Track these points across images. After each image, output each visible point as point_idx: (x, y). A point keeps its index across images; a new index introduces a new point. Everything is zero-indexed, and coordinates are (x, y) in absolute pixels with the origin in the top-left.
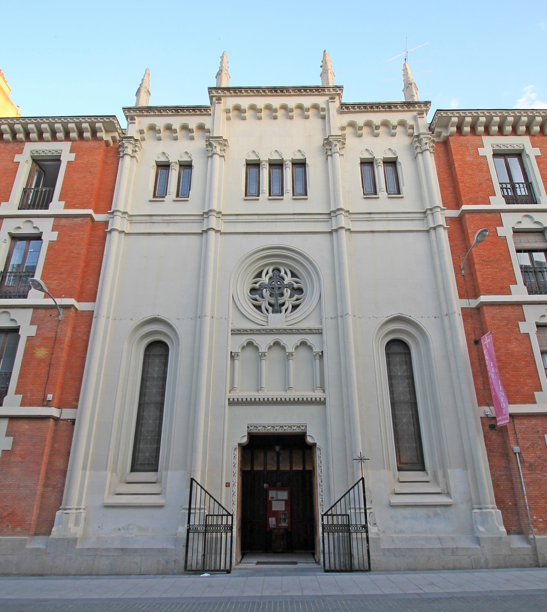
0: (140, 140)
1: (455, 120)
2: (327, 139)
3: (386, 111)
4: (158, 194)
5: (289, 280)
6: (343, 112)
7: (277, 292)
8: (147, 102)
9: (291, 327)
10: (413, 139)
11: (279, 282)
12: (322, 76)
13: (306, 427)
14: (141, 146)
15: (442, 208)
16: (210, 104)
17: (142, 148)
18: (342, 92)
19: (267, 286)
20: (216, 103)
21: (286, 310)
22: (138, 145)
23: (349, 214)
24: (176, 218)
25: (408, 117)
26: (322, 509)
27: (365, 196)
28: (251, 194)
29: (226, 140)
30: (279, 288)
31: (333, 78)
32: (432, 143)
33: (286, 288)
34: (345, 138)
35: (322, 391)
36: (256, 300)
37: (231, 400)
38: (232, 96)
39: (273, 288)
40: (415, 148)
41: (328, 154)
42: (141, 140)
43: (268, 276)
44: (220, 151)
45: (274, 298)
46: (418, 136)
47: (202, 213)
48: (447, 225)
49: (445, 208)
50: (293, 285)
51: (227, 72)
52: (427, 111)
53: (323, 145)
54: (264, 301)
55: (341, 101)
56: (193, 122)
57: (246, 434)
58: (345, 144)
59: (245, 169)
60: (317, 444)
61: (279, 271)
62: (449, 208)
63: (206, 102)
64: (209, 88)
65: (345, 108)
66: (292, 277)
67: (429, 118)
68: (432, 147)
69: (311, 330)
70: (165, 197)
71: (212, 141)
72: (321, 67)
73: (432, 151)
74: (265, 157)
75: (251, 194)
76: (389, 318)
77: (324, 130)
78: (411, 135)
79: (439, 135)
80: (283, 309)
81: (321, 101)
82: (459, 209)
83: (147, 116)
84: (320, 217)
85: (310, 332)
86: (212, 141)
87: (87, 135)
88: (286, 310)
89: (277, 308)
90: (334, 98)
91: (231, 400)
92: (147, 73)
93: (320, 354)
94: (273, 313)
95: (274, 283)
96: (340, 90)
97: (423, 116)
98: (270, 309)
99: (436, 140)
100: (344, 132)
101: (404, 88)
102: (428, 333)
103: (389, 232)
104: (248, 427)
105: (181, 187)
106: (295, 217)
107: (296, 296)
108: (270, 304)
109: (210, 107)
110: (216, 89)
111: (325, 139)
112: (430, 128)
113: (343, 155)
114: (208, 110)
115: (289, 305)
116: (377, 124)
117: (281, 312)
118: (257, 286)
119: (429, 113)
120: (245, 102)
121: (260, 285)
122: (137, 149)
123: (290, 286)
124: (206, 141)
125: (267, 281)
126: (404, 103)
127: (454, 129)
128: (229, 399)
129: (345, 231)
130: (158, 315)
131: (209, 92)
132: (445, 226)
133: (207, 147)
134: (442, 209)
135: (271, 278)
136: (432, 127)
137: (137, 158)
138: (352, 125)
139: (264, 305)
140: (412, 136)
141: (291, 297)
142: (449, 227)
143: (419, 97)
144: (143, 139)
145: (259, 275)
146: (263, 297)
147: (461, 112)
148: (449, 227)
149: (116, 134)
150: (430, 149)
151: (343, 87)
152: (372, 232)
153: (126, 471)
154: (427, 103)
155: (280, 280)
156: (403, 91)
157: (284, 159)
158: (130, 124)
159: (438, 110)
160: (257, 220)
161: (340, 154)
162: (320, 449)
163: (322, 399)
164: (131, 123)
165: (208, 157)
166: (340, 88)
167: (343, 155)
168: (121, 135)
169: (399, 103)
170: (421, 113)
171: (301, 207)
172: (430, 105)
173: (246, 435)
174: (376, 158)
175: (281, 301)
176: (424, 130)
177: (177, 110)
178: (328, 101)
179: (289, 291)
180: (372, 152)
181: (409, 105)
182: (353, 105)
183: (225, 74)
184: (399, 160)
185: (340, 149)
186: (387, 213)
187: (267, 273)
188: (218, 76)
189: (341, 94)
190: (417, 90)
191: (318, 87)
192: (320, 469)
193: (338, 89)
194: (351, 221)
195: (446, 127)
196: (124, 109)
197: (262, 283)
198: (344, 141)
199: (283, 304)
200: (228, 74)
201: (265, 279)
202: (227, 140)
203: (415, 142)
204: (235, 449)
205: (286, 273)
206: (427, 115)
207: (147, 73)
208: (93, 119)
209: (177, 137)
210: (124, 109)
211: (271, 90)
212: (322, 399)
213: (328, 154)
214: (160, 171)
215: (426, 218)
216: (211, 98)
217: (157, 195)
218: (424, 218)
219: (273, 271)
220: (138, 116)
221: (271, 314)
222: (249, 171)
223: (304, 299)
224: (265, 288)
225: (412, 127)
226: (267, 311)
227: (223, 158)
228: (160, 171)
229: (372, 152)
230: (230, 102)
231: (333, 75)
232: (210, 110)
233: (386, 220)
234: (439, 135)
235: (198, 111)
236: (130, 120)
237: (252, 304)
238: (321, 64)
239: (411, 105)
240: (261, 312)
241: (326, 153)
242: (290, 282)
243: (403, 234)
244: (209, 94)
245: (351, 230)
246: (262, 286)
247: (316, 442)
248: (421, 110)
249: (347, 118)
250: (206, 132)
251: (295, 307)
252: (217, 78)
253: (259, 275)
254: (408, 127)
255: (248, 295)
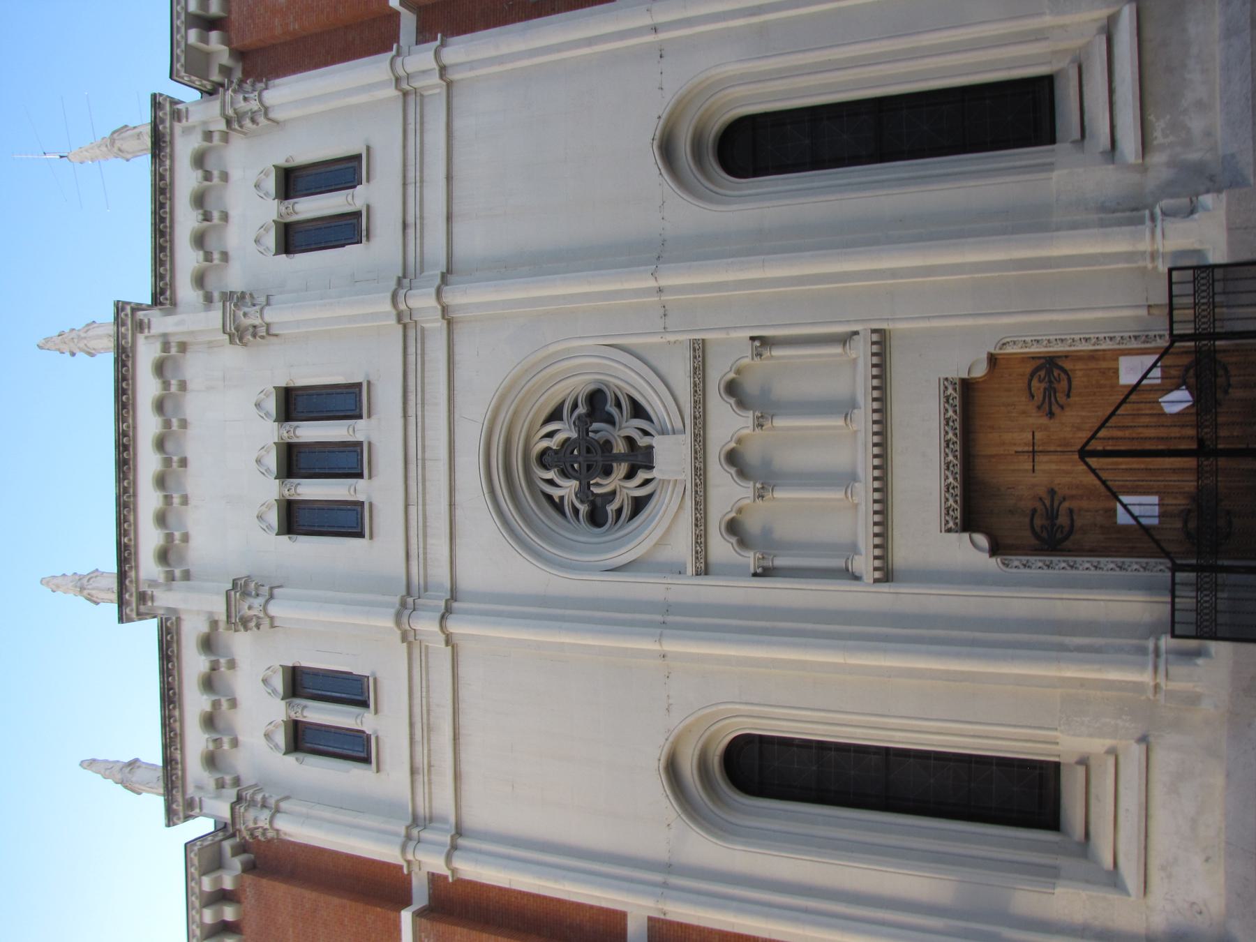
0: (238, 788)
1: (193, 35)
2: (231, 336)
3: (171, 199)
4: (363, 752)
5: (567, 426)
6: (171, 299)
7: (598, 458)
8: (152, 767)
9: (688, 422)
10: (235, 130)
11: (572, 452)
12: (93, 352)
13: (946, 379)
14: (251, 787)
15: (394, 52)
16: (156, 619)
17: (256, 785)
18: (128, 303)
19: (584, 482)
20: (152, 604)
21: (646, 433)
22: (248, 794)
23: (405, 276)
24: (417, 710)
25: (185, 147)
26: (1158, 338)
27: (364, 239)
28: (357, 524)
29: (235, 583)
30: (588, 451)
31: (98, 327)
32: (245, 85)
33: (587, 434)
34: (231, 292)
35: (855, 337)
36: (619, 512)
37: (878, 575)
38: (137, 567)
39: (589, 467)
40: (255, 126)
41: (264, 334)
42: (239, 786)
43: (558, 481)
44: (260, 598)
45: (615, 465)
46: (229, 122)
47: (405, 644)
48: (436, 39)
49: (395, 46)
50: (579, 417)
51: (84, 576)
52: (174, 102)
53: (245, 345)
54: (621, 491)
55: (148, 306)
56: (194, 664)
57: (966, 536)
58: (243, 293)
59: (298, 536)
60: (993, 351)
61: (545, 451)
62: (395, 37)
63: (151, 627)
64: (121, 620)
65: (163, 295)
66: (561, 419)
67: (188, 95)
68: (253, 85)
69: (695, 368)
70: (368, 735)
71: (236, 616)
72: (73, 354)
73: (262, 85)
74: (270, 490)
75: (357, 524)
76: (663, 171)
77: (211, 345)
78: (225, 138)
79: (226, 71)
80: (642, 441)
81: (146, 354)
82: (398, 14)
83: (184, 770)
84: (411, 350)
85: (700, 371)
86: (236, 616)
87: (229, 913)
88: (646, 433)
89: (640, 459)
90: (141, 322)
91: (878, 575)
92: (90, 764)
93: (757, 343)
94: (653, 467)
95: (576, 466)
96: (123, 309)
97: (184, 110)
98: (642, 475)
99: (238, 74)
100: (216, 295)
101: (123, 157)
102: (689, 200)
103: (449, 178)
104: (949, 530)
105: (343, 695)
106: (411, 411)
107: (611, 408)
108: (630, 475)
109: (162, 618)
110: (122, 603)
111: (232, 341)
112: (210, 93)
113: (268, 296)
114: (168, 624)
115: (631, 427)
116: (200, 217)
117: (650, 448)
118: (583, 509)
119: (177, 97)
120: (149, 539)
121: (582, 502)
122: (259, 797)
123: (583, 424)
124: (236, 631)
125: (574, 484)
126: (154, 156)
127: (214, 35)
128: (876, 581)
129: (447, 285)
130: (659, 760)
131: (130, 620)
132: (438, 43)
133: (251, 629)
134: (398, 54)
135: (564, 474)
136: (209, 87)
137: (279, 797)
138: (200, 280)
139: (632, 489)
140: (227, 133)
141: (610, 420)
142: (439, 35)
143: (143, 117)
144: (237, 781)
145: (558, 506)
146: (613, 493)
147: (178, 23)
148: (439, 35)
149: (227, 846)
150: (259, 89)
151: (118, 301)
152: (449, 218)
153: (1057, 843)
154: (156, 102)
155: (569, 452)
156: (128, 160)
157: (277, 441)
158: (205, 811)
159: (171, 77)
160: (420, 507)
161: (265, 303)
162: (1004, 344)
163: (875, 337)
164: (201, 809)
165: (272, 626)
166: (120, 307)
167: (268, 296)
168: (228, 834)
169: (153, 168)
170: (177, 116)
171: (387, 398)
172: (161, 95)
173: (970, 537)
174: (275, 217)
175: (620, 447)
176: (215, 106)
177: (170, 698)
178: (146, 338)
179: (596, 426)
180: (262, 227)
181: (159, 144)
182: (158, 276)
183: (91, 582)
184: (281, 161)
185: (254, 305)
186: (405, 185)
187: (551, 482)
188: (94, 599)
189: (132, 305)
190: (126, 126)
191: (117, 361)
192: (1055, 342)
193: (122, 315)
194: (422, 271)
195: (208, 55)
196: (170, 823)
197: (576, 495)
198: (235, 296)
199: (630, 440)
200: (88, 574)
201: (567, 489)
202: (234, 580)
203: (241, 126)
204: (1004, 564)
205: (550, 435)
206: (181, 102)
207: (90, 764)
208: (199, 900)
209: (229, 699)
210: (170, 823)
211: (124, 472)
212: (875, 337)
213: (264, 334)
214: (309, 745)
215: (417, 91)
216: (141, 616)
217: (363, 755)
218: (418, 94)
219: (546, 467)
220: (184, 793)
221: (655, 473)
222: (304, 528)
223: (618, 387)
224: (589, 488)
225: (208, 135)
226: (647, 482)
227: (276, 591)
228: (309, 745)
229: (262, 227)
230: (148, 567)
231: (91, 327)
232: (167, 619)
233: (421, 187)
234: (226, 71)
235: (170, 649)
236: (192, 810)
237: (628, 522)
238: (68, 354)
239: (159, 140)
240: (649, 497)
241: (262, 337)
242: (574, 423)
243: (457, 145)
244: (132, 620)
245: (445, 271)
246: (584, 493)
247: (985, 356)
248: (170, 114)
249: (185, 291)
250: (217, 630)
251: (638, 411)
252: (99, 601)
253: (558, 506)
254: (206, 144)
255: (609, 529)
